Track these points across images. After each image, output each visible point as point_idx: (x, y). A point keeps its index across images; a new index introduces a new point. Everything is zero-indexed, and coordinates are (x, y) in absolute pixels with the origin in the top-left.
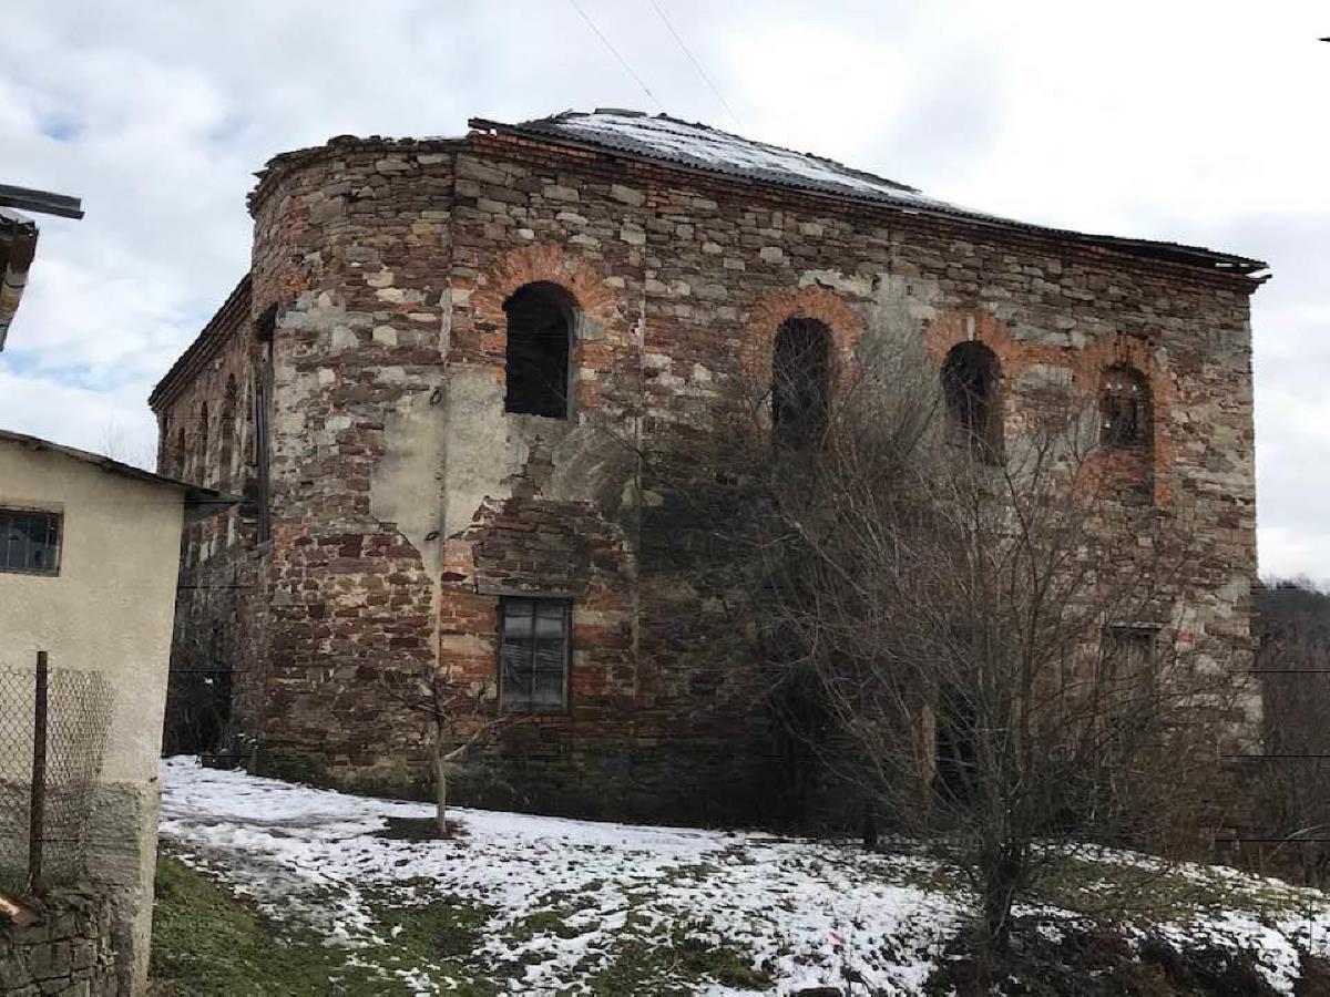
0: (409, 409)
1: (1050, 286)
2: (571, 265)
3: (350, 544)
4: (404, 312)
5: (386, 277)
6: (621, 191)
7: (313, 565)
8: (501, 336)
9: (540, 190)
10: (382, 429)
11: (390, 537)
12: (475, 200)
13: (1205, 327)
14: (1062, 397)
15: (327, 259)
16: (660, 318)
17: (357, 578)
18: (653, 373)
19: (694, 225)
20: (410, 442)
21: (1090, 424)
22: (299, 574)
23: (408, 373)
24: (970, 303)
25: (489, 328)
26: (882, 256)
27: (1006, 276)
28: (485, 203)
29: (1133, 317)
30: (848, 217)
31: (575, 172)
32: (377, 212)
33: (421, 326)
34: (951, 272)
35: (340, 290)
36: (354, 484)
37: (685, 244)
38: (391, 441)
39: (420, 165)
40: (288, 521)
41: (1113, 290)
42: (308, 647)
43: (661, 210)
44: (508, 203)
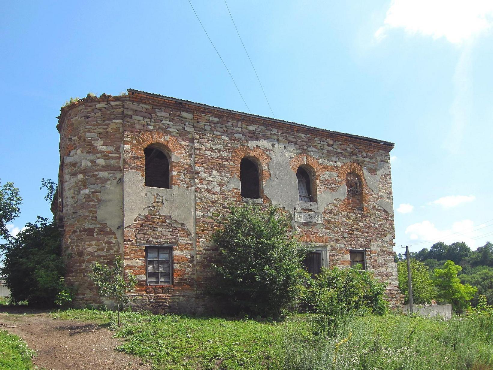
0: (109, 186)
1: (329, 148)
2: (168, 138)
3: (90, 232)
4: (107, 154)
5: (100, 142)
6: (184, 114)
7: (78, 239)
8: (143, 161)
9: (155, 113)
10: (100, 192)
11: (104, 228)
12: (131, 116)
13: (377, 161)
14: (334, 182)
15: (80, 138)
16: (200, 155)
17: (94, 243)
18: (198, 173)
19: (210, 126)
20: (111, 196)
21: (344, 189)
22: (74, 243)
23: (109, 174)
24: (304, 152)
25: (138, 158)
26: (275, 137)
27: (315, 144)
28: (135, 117)
29: (355, 158)
30: (264, 124)
31: (167, 107)
32: (96, 121)
33: (113, 158)
34: (298, 143)
35: (84, 148)
36: (91, 212)
37: (207, 132)
38: (105, 197)
39: (112, 106)
40: (69, 226)
41: (349, 150)
42: (78, 266)
43: (199, 120)
44: (144, 117)
